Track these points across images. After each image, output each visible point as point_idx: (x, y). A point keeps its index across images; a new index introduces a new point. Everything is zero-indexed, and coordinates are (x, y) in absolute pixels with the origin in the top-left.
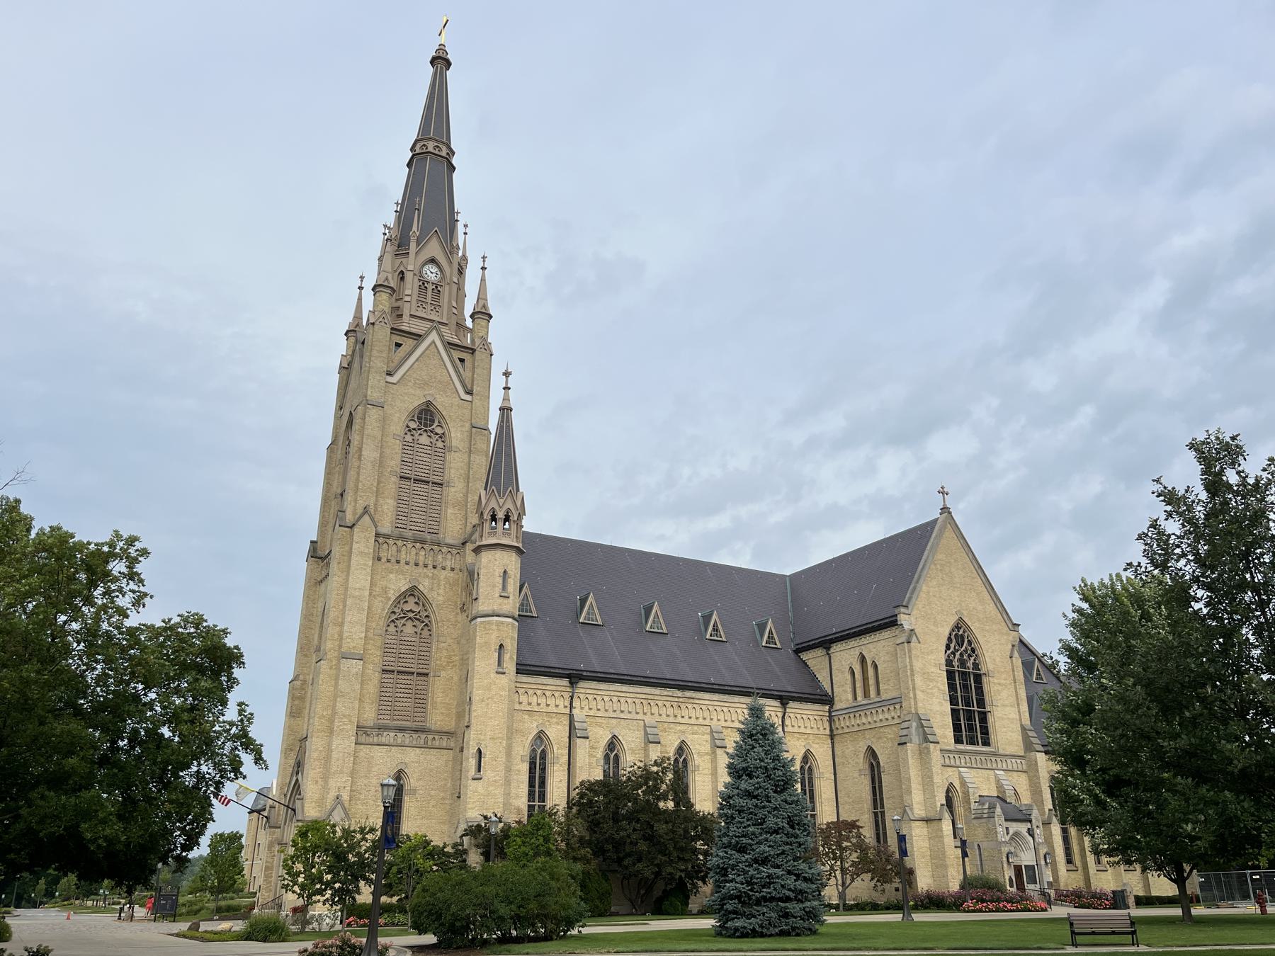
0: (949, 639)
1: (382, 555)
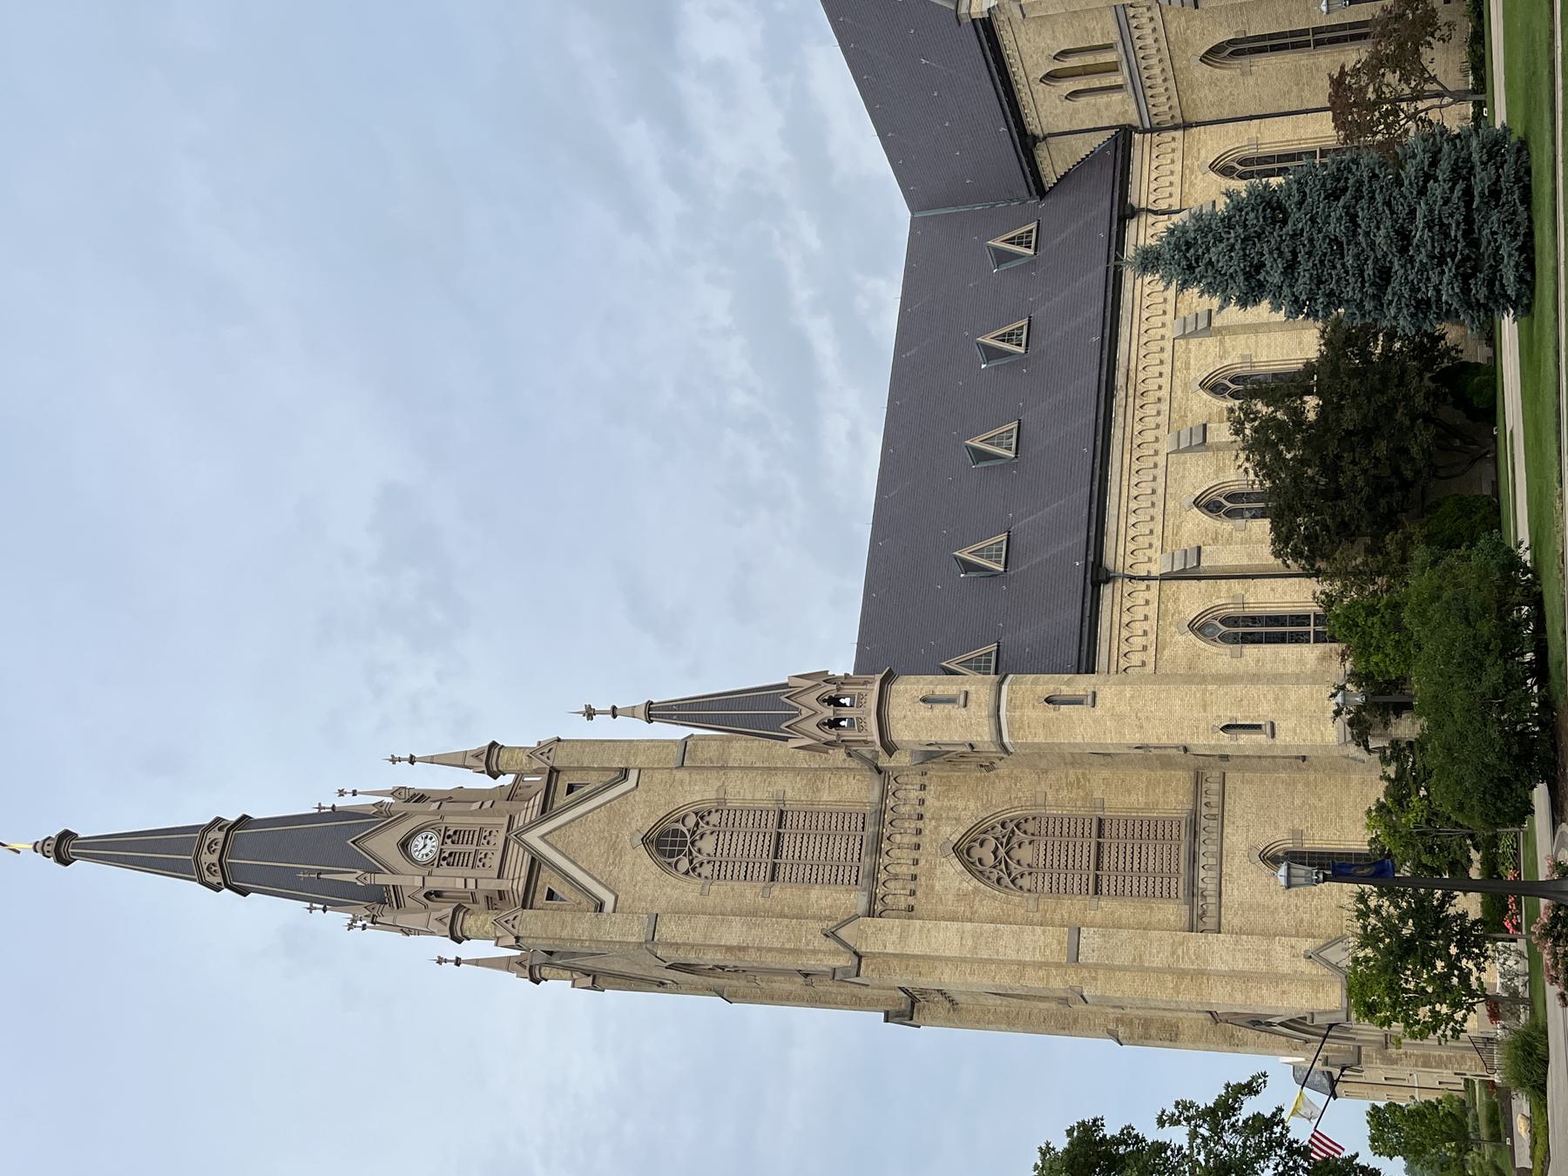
1: (903, 905)
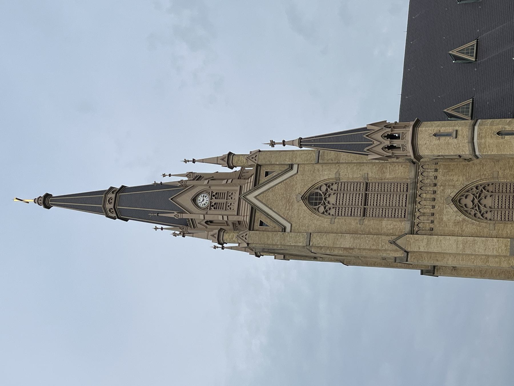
1: (428, 228)
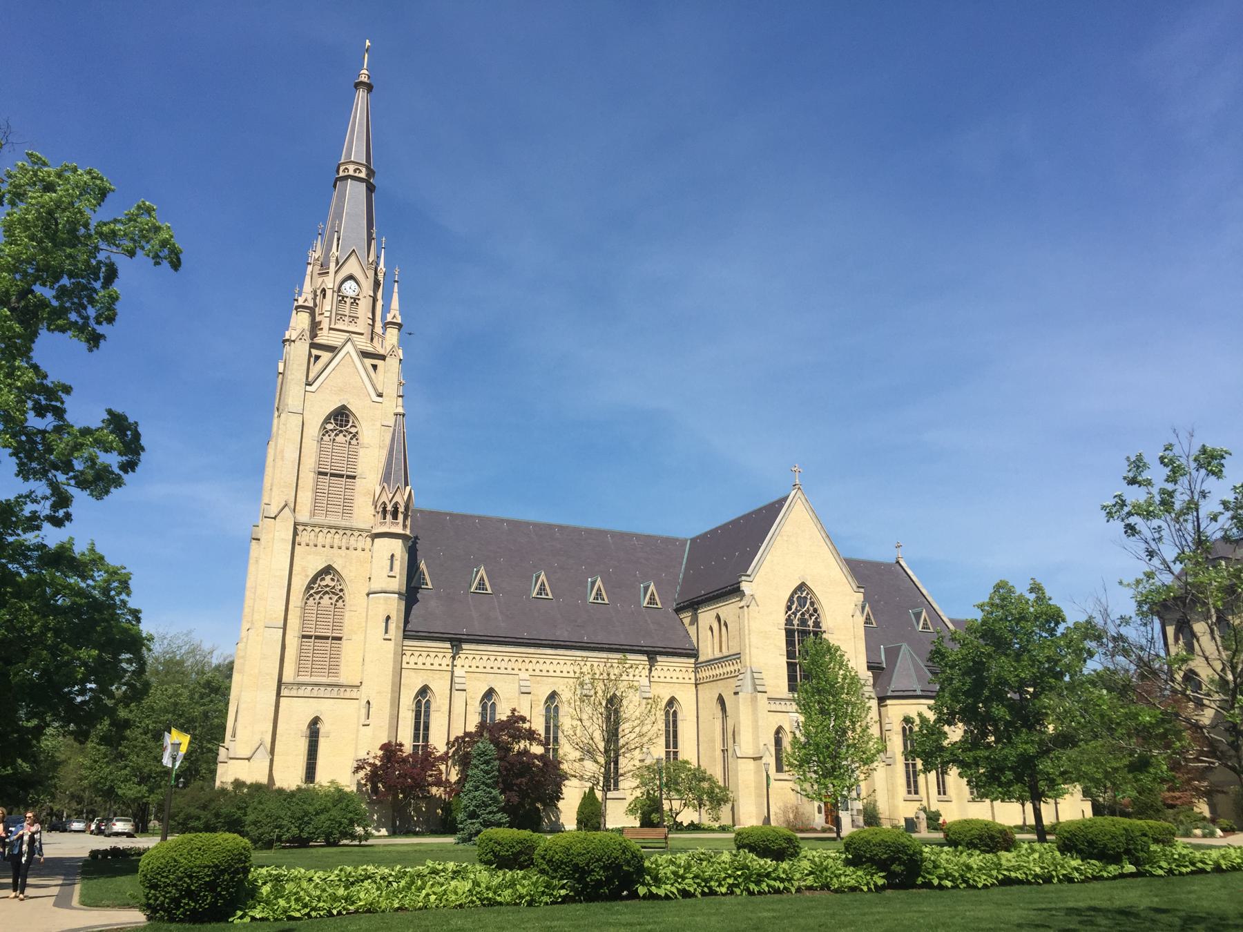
0: (791, 600)
